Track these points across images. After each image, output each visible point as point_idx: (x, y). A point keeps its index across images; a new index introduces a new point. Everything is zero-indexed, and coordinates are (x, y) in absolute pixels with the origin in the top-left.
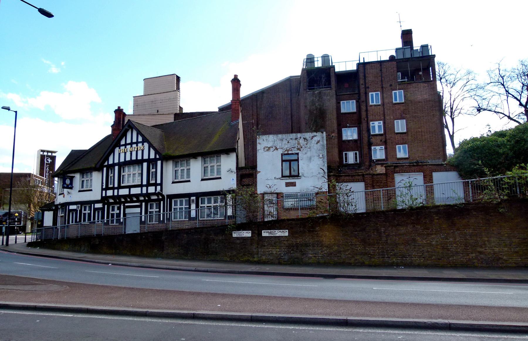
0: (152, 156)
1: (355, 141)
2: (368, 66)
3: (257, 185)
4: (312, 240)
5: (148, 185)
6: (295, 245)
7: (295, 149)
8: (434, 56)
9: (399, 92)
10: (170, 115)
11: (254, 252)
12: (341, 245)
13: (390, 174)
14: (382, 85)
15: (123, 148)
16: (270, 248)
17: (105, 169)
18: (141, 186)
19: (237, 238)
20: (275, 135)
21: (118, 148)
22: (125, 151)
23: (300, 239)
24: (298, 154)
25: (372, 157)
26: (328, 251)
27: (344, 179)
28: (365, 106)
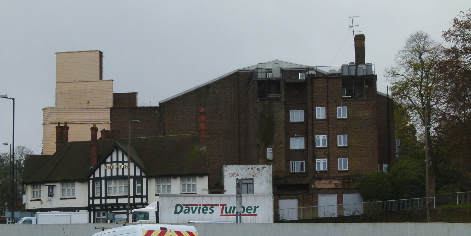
0: (138, 174)
1: (301, 151)
5: (135, 196)
8: (376, 76)
9: (342, 108)
10: (105, 110)
15: (109, 165)
17: (91, 181)
18: (128, 197)
20: (237, 165)
21: (104, 164)
22: (112, 168)
24: (253, 179)
25: (315, 168)
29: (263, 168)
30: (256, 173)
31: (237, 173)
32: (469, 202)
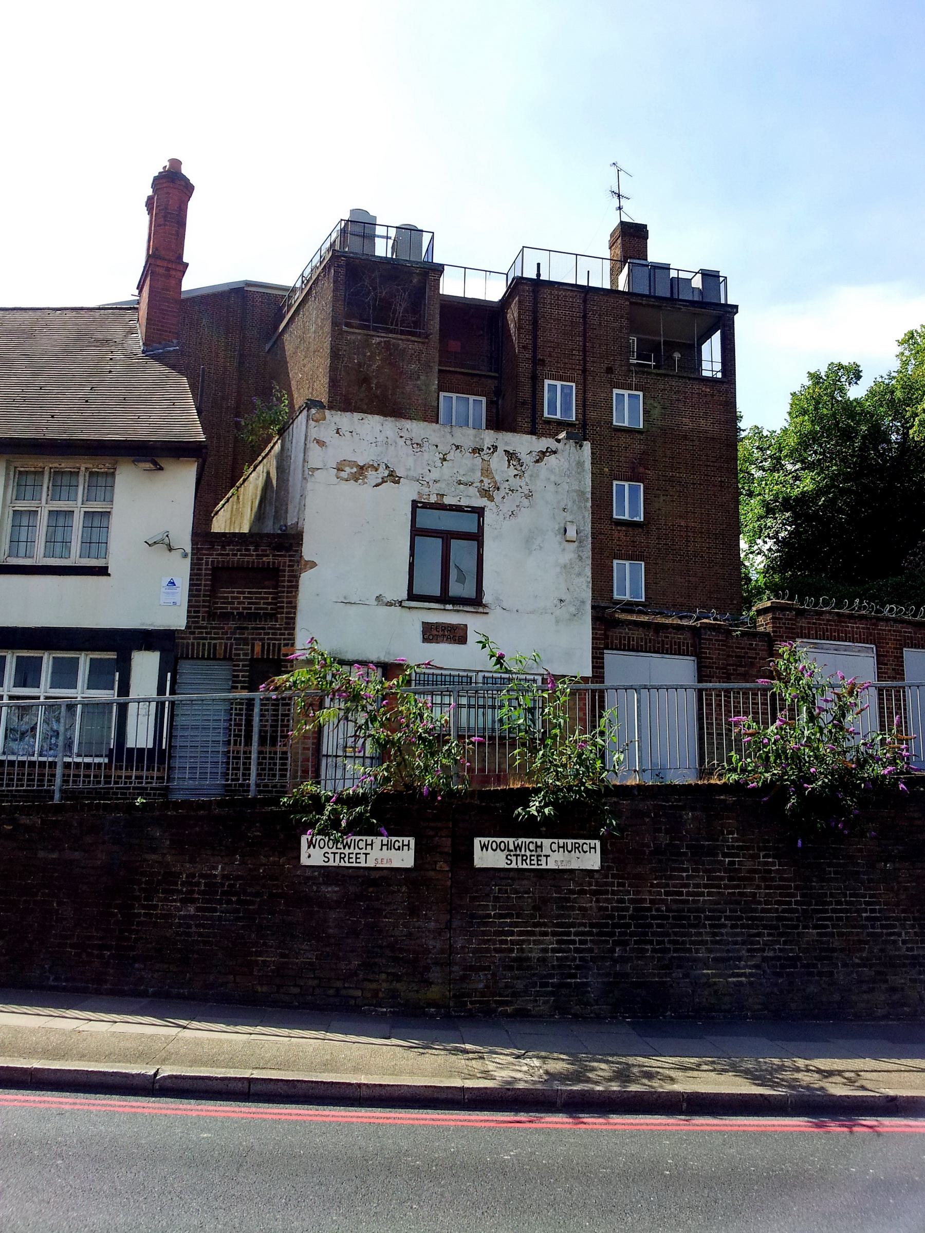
2: (545, 292)
3: (294, 618)
4: (709, 894)
6: (631, 917)
7: (473, 491)
11: (428, 951)
12: (830, 919)
13: (782, 637)
14: (585, 363)
16: (512, 933)
19: (328, 874)
23: (658, 886)
24: (479, 512)
26: (781, 950)
27: (629, 638)
28: (529, 420)
29: (543, 454)
30: (497, 478)
31: (387, 467)
32: (492, 738)
